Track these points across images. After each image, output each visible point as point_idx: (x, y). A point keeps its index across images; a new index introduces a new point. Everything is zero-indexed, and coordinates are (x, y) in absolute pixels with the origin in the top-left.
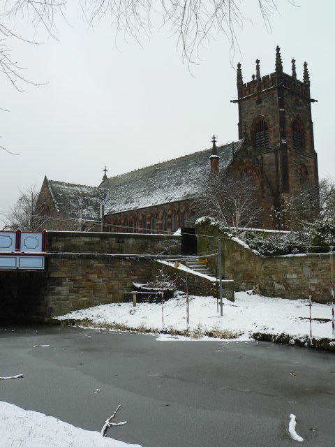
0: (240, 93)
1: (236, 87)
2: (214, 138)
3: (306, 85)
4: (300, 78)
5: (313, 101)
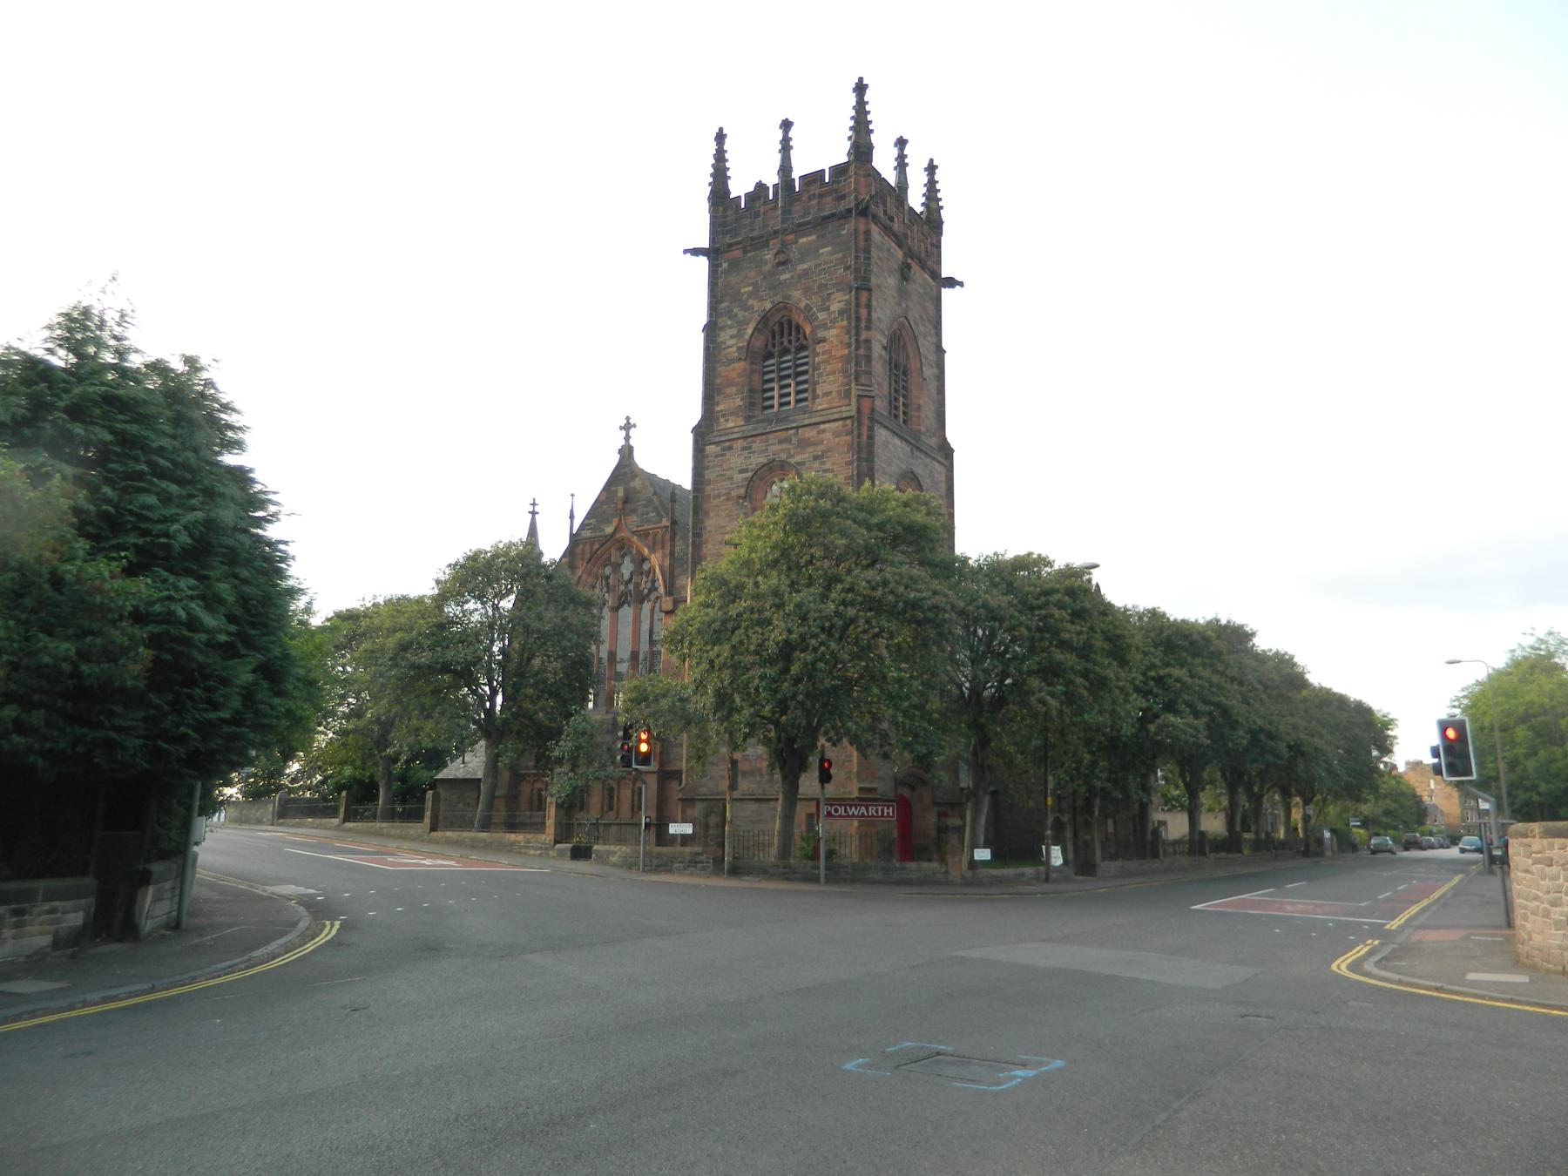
0: (719, 226)
1: (706, 205)
2: (534, 504)
3: (931, 222)
4: (916, 200)
5: (951, 282)
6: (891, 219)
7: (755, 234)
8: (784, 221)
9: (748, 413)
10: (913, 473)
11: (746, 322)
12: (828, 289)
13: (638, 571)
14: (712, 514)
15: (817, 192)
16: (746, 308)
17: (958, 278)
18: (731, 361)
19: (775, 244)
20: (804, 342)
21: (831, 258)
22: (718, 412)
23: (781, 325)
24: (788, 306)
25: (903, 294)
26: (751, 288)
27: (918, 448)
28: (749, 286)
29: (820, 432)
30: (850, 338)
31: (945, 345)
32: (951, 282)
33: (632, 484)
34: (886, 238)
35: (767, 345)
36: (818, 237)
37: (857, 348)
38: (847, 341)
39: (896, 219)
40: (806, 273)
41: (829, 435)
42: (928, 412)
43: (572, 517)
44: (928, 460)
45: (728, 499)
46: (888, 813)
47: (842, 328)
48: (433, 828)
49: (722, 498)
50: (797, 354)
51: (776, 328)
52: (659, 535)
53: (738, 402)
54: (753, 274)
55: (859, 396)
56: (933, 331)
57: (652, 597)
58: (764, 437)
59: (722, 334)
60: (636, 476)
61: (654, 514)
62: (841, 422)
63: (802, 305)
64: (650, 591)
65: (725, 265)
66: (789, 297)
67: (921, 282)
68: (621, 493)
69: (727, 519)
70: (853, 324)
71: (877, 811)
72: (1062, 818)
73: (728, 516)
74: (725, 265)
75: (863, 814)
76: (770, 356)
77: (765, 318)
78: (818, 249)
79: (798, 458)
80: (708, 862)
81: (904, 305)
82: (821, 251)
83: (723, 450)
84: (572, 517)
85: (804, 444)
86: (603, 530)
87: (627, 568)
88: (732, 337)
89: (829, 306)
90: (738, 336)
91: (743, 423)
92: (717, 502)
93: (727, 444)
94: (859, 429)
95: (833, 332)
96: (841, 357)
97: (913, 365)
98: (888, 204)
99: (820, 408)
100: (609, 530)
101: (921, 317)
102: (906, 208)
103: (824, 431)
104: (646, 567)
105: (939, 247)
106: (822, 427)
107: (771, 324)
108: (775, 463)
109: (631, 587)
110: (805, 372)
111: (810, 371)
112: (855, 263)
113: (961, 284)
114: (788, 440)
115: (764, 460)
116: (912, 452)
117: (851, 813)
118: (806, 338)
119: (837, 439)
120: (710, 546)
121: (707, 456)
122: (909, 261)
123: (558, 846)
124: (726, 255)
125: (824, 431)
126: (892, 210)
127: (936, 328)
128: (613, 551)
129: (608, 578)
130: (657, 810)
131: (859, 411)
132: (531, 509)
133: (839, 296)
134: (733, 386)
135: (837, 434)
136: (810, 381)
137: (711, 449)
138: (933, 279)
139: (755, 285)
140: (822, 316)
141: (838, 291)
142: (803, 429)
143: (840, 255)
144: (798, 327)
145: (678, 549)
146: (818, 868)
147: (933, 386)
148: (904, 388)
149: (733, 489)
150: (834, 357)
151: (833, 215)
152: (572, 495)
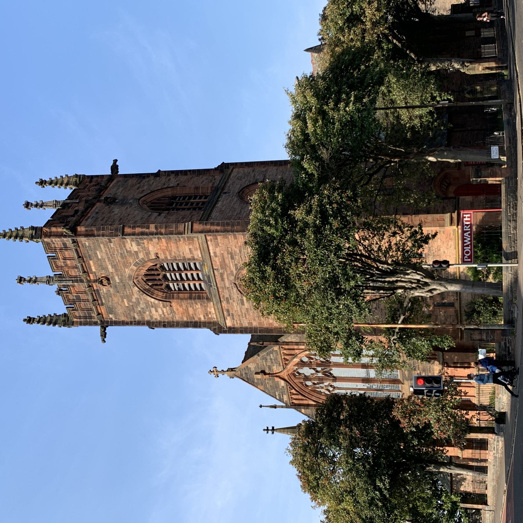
2: (268, 430)
5: (115, 167)
6: (77, 211)
7: (90, 298)
8: (82, 281)
10: (239, 192)
11: (147, 303)
12: (124, 253)
13: (309, 365)
16: (138, 303)
17: (111, 163)
18: (172, 311)
20: (158, 266)
21: (104, 251)
22: (205, 318)
24: (136, 277)
25: (124, 202)
26: (125, 300)
27: (223, 189)
28: (123, 301)
30: (155, 238)
31: (155, 171)
32: (115, 167)
33: (253, 369)
34: (89, 215)
36: (91, 260)
37: (162, 234)
38: (157, 240)
39: (76, 208)
40: (114, 266)
41: (218, 250)
42: (198, 181)
43: (275, 407)
44: (230, 182)
46: (468, 217)
47: (148, 243)
48: (486, 504)
50: (166, 270)
51: (150, 284)
52: (285, 352)
53: (199, 306)
54: (116, 299)
55: (191, 232)
56: (147, 179)
58: (220, 290)
59: (155, 317)
60: (247, 367)
61: (271, 355)
62: (209, 243)
63: (135, 268)
65: (111, 316)
66: (130, 277)
67: (115, 189)
68: (259, 376)
70: (145, 237)
71: (467, 225)
72: (468, 90)
74: (111, 316)
75: (469, 234)
77: (144, 291)
79: (233, 269)
80: (505, 339)
81: (131, 201)
82: (100, 257)
83: (229, 315)
84: (275, 407)
85: (224, 265)
86: (283, 387)
87: (307, 371)
88: (157, 311)
89: (135, 252)
90: (156, 307)
91: (212, 303)
93: (225, 313)
94: (213, 232)
95: (151, 248)
96: (167, 243)
97: (169, 193)
98: (67, 214)
99: (200, 256)
101: (138, 188)
102: (69, 201)
104: (306, 359)
105: (92, 177)
106: (212, 254)
107: (148, 287)
109: (319, 369)
110: (178, 265)
111: (177, 262)
112: (107, 236)
113: (115, 161)
114: (222, 275)
115: (235, 290)
116: (226, 193)
117: (469, 243)
118: (156, 265)
119: (220, 245)
122: (103, 198)
123: (496, 432)
124: (104, 316)
125: (215, 253)
126: (71, 212)
127: (144, 178)
129: (314, 384)
130: (469, 352)
131: (201, 232)
132: (270, 432)
133: (128, 246)
134: (188, 309)
135: (217, 245)
136: (183, 262)
137: (229, 323)
138: (113, 180)
140: (141, 256)
141: (125, 247)
142: (214, 266)
143: (102, 246)
144: (149, 270)
146: (507, 267)
147: (183, 178)
148: (184, 199)
150: (167, 247)
151: (76, 250)
152: (261, 406)
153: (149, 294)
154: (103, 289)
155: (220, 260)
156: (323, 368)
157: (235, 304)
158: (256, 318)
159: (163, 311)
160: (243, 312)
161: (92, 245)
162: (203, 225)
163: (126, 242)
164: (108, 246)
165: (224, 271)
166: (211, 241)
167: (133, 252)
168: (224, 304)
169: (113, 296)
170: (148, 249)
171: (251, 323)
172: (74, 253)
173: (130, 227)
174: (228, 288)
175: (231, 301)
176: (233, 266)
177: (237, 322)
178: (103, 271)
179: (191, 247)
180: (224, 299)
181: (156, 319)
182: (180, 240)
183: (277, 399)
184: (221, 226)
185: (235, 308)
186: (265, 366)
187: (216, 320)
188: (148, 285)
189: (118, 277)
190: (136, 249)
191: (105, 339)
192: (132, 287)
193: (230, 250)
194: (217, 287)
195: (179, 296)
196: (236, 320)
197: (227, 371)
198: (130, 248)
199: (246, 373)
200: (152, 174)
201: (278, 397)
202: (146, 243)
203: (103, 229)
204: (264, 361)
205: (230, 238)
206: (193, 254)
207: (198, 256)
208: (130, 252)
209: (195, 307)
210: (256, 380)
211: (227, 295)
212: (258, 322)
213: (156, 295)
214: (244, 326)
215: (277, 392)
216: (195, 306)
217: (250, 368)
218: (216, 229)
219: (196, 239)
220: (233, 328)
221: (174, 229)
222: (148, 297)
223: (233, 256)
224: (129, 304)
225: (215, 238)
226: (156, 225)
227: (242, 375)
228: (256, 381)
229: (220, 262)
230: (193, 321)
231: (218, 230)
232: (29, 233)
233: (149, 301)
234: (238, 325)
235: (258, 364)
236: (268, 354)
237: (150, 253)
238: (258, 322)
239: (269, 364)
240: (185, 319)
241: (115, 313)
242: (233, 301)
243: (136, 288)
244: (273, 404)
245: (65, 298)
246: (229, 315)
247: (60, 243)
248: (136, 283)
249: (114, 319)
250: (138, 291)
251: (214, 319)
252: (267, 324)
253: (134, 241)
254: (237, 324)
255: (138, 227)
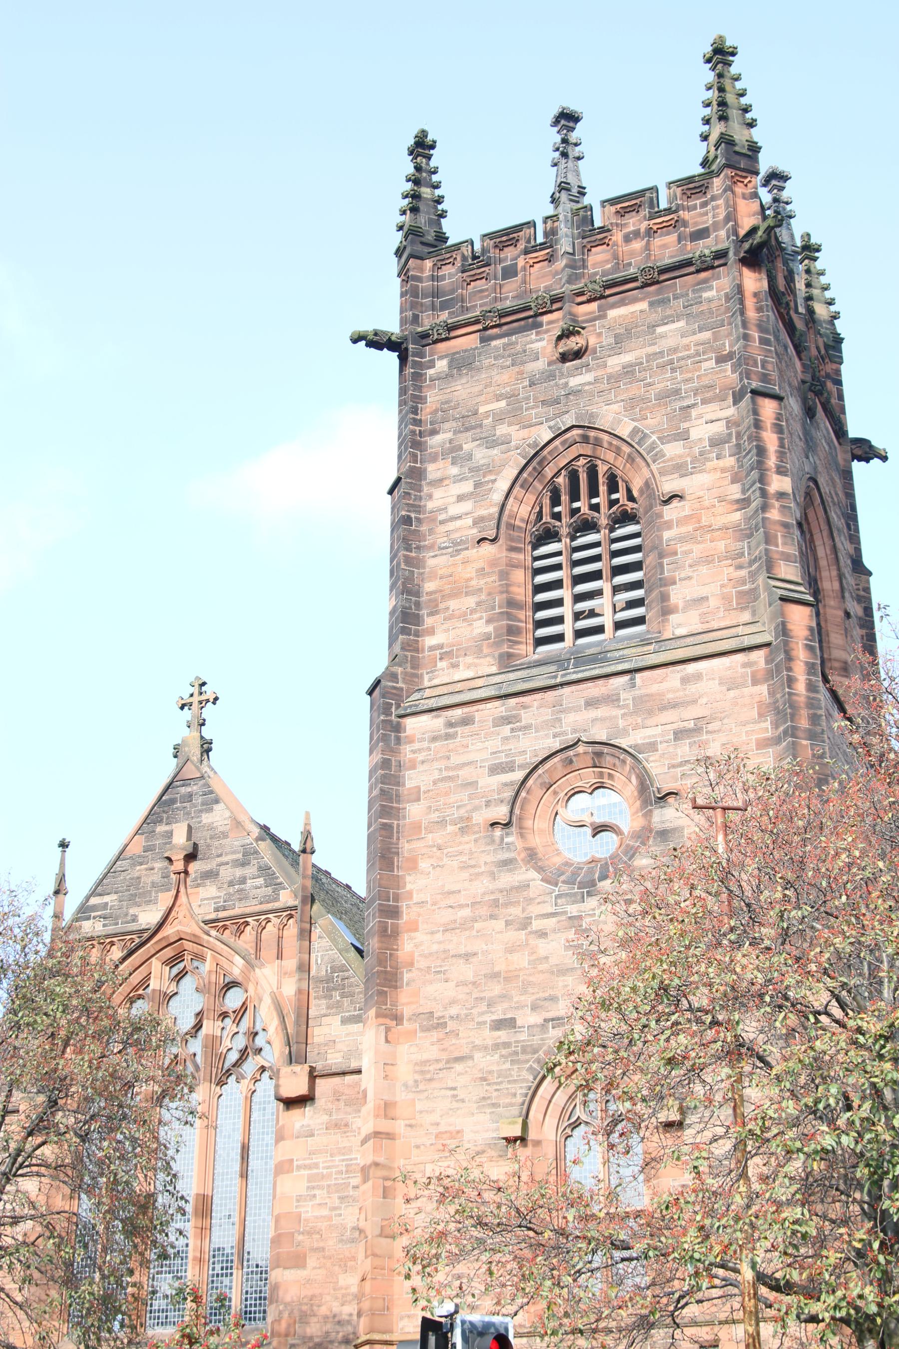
9: (505, 649)
11: (491, 469)
14: (423, 865)
15: (643, 226)
16: (491, 442)
18: (458, 546)
19: (554, 322)
21: (686, 341)
22: (432, 648)
23: (573, 477)
26: (503, 404)
28: (498, 398)
29: (685, 680)
31: (868, 561)
33: (206, 818)
35: (540, 515)
36: (651, 304)
40: (628, 371)
45: (463, 831)
47: (723, 470)
49: (450, 828)
53: (481, 627)
57: (250, 1067)
58: (551, 694)
59: (438, 493)
60: (217, 801)
61: (261, 881)
62: (739, 657)
64: (244, 1054)
68: (180, 837)
69: (465, 875)
73: (464, 867)
76: (549, 535)
78: (653, 327)
82: (659, 330)
86: (135, 919)
88: (461, 498)
89: (687, 431)
92: (437, 837)
93: (458, 712)
99: (680, 632)
100: (149, 917)
103: (698, 677)
106: (691, 668)
107: (549, 472)
108: (581, 749)
114: (612, 699)
118: (631, 498)
119: (732, 693)
120: (419, 936)
121: (410, 740)
124: (441, 346)
125: (698, 677)
128: (156, 964)
133: (713, 410)
134: (467, 594)
135: (731, 684)
139: (511, 397)
140: (673, 450)
141: (704, 402)
145: (316, 957)
149: (476, 808)
150: (709, 529)
152: (64, 845)
153: (525, 475)
154: (540, 340)
155: (670, 696)
156: (198, 1059)
157: (494, 743)
158: (437, 814)
159: (460, 517)
160: (460, 773)
161: (704, 307)
162: (807, 639)
163: (724, 404)
164: (704, 353)
165: (627, 706)
166: (745, 665)
167: (685, 425)
168: (497, 708)
169: (516, 369)
170: (700, 472)
171: (418, 799)
172: (672, 257)
173: (778, 419)
174: (560, 720)
175: (506, 730)
176: (649, 737)
177: (420, 750)
178: (612, 340)
179: (713, 603)
180: (514, 709)
181: (430, 496)
182: (739, 567)
183: (88, 899)
184: (808, 698)
185: (480, 745)
186: (219, 860)
187: (426, 683)
188: (557, 474)
189: (589, 383)
190: (694, 434)
191: (364, 342)
192: (552, 423)
193: (711, 727)
194: (562, 685)
195: (517, 567)
196: (429, 749)
197: (202, 737)
198: (700, 417)
199: (190, 796)
200: (858, 551)
201: (94, 901)
202: (721, 463)
203: (763, 341)
204: (240, 856)
205: (763, 725)
206: (686, 609)
207: (679, 625)
208: (687, 418)
209: (475, 616)
210: (167, 828)
211: (526, 717)
212: (420, 822)
213: (520, 497)
214: (408, 774)
215: (114, 897)
216: (481, 618)
217: (211, 810)
218: (797, 680)
219: (746, 616)
220: (398, 739)
221: (780, 549)
222: (516, 472)
223: (689, 738)
224: (487, 417)
225: (760, 676)
226: (787, 494)
227: (186, 782)
228: (161, 828)
229: (661, 695)
230: (424, 612)
231: (794, 686)
232: (740, 135)
233: (498, 473)
234: (410, 756)
235: (225, 835)
236: (264, 870)
237: (682, 476)
238: (420, 822)
239: (226, 873)
240: (429, 586)
241: (452, 376)
242: (506, 738)
243: (547, 435)
244: (69, 884)
245: (507, 234)
246: (450, 725)
247: (706, 222)
248: (568, 435)
249: (431, 372)
250: (535, 444)
251: (430, 680)
252: (410, 851)
253: (728, 428)
254: (414, 752)
255: (781, 440)
